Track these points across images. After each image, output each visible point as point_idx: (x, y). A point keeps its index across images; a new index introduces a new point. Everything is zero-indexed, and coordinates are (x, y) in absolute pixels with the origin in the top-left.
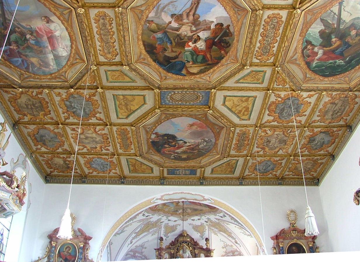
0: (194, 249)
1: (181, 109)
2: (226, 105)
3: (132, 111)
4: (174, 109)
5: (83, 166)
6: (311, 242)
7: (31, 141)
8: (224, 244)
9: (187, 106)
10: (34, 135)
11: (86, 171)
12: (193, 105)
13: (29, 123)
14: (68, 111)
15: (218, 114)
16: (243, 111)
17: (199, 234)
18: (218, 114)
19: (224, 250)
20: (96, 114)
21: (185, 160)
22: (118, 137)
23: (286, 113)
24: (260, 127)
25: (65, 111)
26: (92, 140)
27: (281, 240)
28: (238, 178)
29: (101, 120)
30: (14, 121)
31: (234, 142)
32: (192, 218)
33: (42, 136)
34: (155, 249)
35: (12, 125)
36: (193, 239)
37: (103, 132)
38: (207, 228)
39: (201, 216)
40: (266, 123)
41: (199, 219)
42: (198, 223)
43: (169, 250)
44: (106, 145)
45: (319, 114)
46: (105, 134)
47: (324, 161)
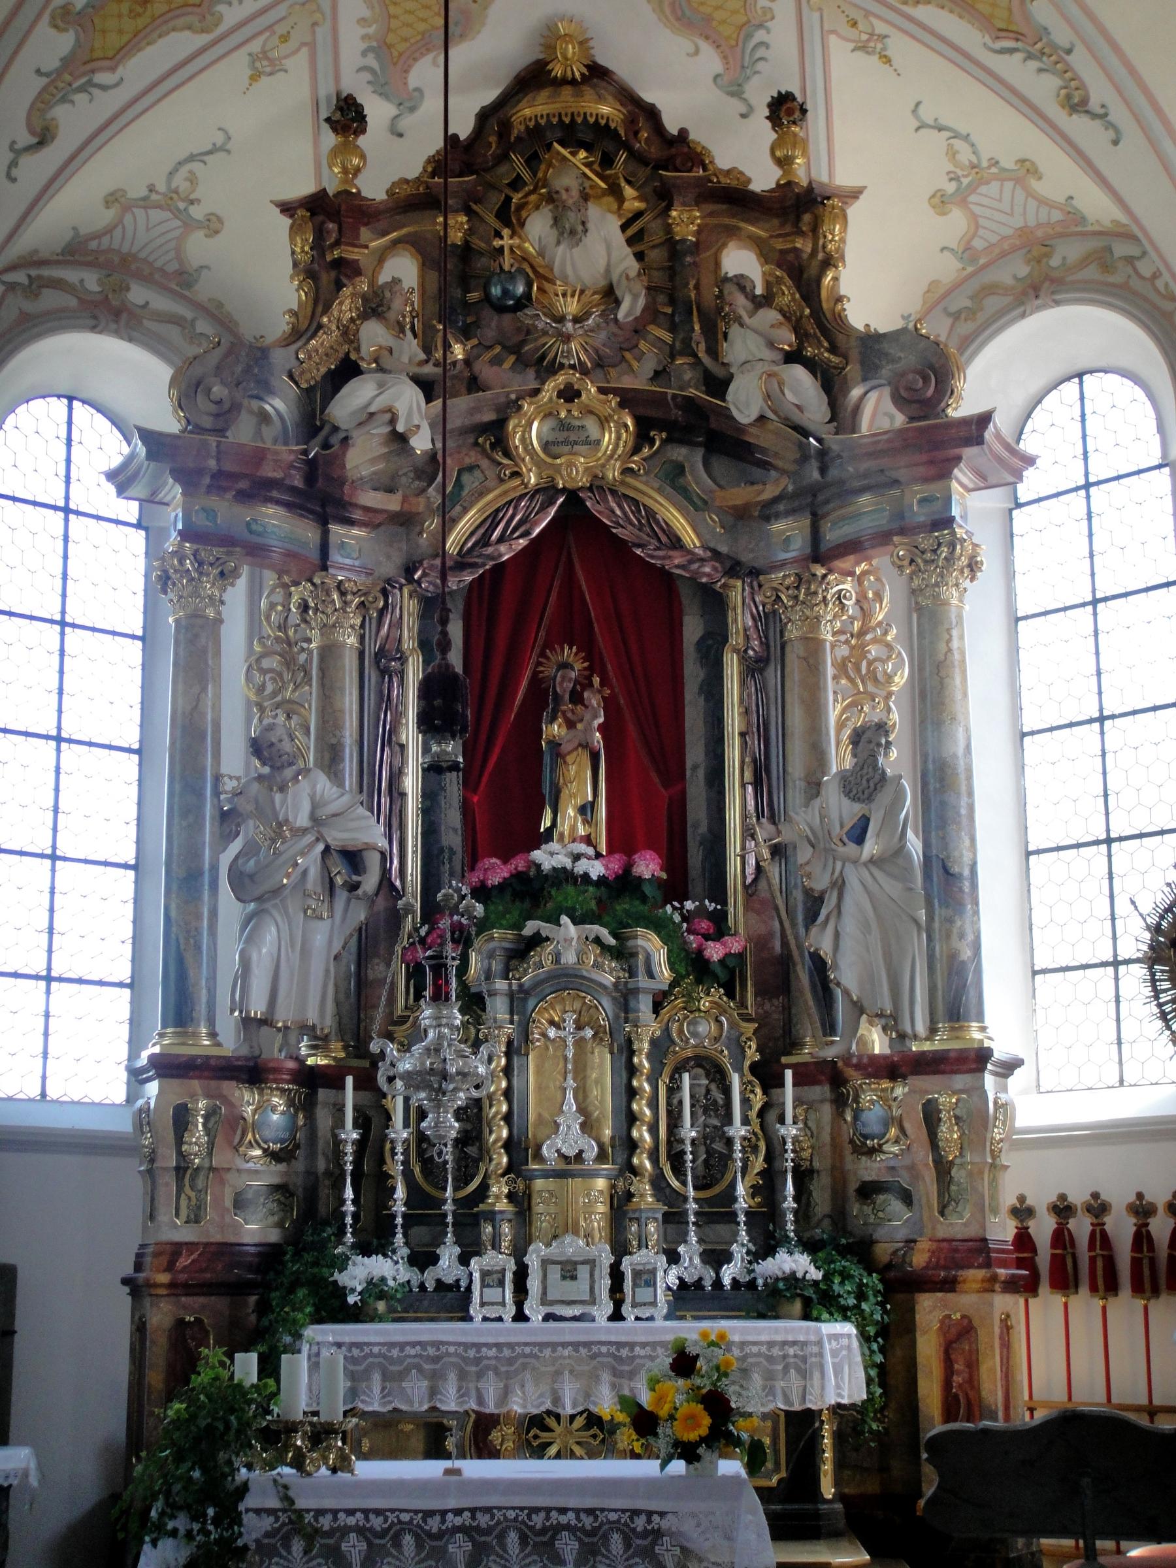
0: (663, 197)
8: (952, 154)
17: (710, 61)
19: (956, 223)
34: (287, 208)
36: (652, 114)
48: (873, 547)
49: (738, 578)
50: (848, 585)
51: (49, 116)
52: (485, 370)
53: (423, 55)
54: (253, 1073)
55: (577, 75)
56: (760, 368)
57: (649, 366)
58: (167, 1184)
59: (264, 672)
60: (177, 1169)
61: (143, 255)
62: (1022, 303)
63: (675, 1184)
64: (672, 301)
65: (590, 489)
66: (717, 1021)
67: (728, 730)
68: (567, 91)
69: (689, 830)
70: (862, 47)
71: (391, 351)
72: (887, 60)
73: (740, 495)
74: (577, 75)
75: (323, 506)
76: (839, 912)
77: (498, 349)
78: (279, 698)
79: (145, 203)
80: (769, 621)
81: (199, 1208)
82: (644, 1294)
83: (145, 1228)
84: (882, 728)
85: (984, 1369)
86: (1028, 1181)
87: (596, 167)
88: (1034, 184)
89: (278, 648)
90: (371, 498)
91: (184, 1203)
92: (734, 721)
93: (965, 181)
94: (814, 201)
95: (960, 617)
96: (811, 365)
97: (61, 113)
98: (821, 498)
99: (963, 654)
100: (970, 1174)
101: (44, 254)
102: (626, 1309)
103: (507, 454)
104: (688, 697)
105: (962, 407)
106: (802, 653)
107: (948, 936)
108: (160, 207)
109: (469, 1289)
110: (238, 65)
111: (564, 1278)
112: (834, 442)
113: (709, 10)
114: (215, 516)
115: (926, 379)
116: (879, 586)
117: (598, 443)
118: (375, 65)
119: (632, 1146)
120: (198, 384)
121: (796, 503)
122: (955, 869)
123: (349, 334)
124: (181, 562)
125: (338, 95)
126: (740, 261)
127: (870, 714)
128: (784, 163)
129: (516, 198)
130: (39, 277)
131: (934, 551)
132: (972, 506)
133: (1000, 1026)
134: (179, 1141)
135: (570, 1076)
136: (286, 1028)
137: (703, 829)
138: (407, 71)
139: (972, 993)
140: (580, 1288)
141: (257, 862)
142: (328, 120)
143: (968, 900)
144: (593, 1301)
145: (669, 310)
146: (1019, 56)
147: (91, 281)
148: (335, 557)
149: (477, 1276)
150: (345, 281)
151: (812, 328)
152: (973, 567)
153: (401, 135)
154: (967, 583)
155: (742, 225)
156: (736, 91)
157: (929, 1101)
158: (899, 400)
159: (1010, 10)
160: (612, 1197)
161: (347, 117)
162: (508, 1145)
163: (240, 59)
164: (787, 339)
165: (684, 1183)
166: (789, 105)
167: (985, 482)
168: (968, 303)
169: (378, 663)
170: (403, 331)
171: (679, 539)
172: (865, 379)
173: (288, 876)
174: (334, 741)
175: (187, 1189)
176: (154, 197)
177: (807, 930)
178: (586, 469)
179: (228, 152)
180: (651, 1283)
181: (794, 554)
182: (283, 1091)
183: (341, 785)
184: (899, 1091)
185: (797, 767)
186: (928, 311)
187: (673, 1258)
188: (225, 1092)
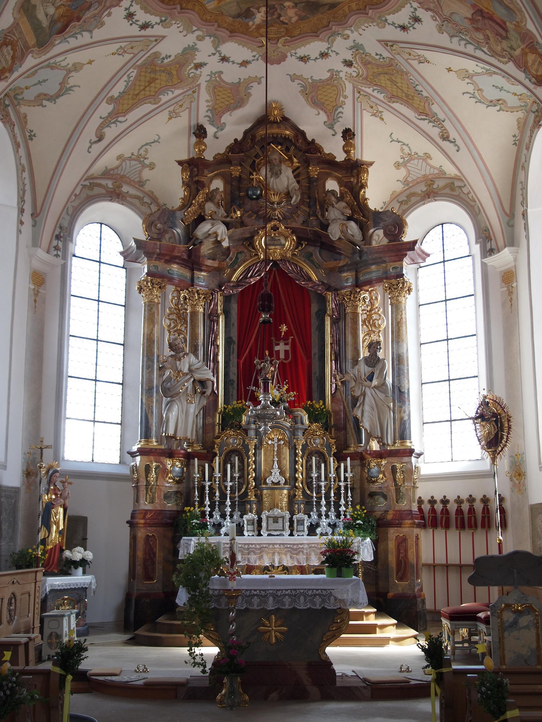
0: (307, 163)
8: (402, 150)
17: (323, 117)
19: (402, 172)
32: (301, 52)
34: (180, 163)
36: (303, 133)
38: (349, 87)
39: (330, 39)
41: (324, 55)
42: (318, 71)
48: (376, 283)
49: (330, 291)
50: (367, 295)
51: (103, 131)
52: (246, 220)
53: (226, 112)
54: (171, 455)
55: (279, 121)
56: (340, 222)
57: (301, 220)
58: (143, 491)
59: (170, 319)
60: (146, 485)
61: (127, 176)
62: (424, 200)
63: (309, 492)
64: (309, 198)
65: (281, 260)
66: (323, 438)
67: (326, 342)
68: (275, 125)
69: (313, 375)
70: (374, 115)
71: (216, 213)
72: (383, 119)
73: (332, 264)
74: (279, 121)
75: (193, 265)
76: (364, 404)
77: (250, 212)
78: (175, 329)
79: (130, 159)
80: (341, 307)
81: (153, 498)
82: (300, 528)
83: (134, 505)
84: (378, 343)
85: (409, 552)
86: (424, 491)
87: (284, 151)
88: (429, 161)
89: (175, 312)
90: (209, 263)
91: (148, 497)
92: (328, 339)
93: (406, 159)
94: (358, 166)
95: (405, 307)
96: (356, 221)
97: (106, 130)
98: (359, 266)
99: (406, 319)
100: (407, 489)
101: (95, 175)
102: (295, 532)
103: (254, 248)
104: (313, 331)
105: (407, 238)
106: (352, 317)
107: (400, 412)
108: (135, 160)
109: (243, 526)
110: (165, 115)
111: (274, 522)
112: (365, 248)
113: (324, 101)
114: (158, 268)
115: (395, 228)
116: (376, 295)
117: (284, 245)
118: (210, 115)
119: (296, 479)
120: (152, 223)
121: (351, 267)
122: (403, 390)
123: (201, 206)
124: (147, 284)
125: (198, 124)
126: (332, 185)
127: (374, 338)
128: (347, 152)
129: (257, 161)
130: (93, 183)
131: (397, 285)
132: (408, 269)
133: (415, 442)
134: (147, 476)
135: (275, 457)
136: (180, 439)
137: (317, 375)
138: (221, 117)
139: (408, 431)
140: (279, 525)
141: (171, 384)
142: (194, 133)
143: (407, 400)
144: (283, 530)
145: (308, 201)
146: (427, 121)
147: (110, 184)
148: (196, 281)
149: (245, 522)
150: (200, 188)
151: (357, 209)
152: (409, 290)
153: (217, 138)
154: (407, 296)
155: (333, 172)
156: (331, 127)
157: (393, 466)
158: (386, 234)
159: (425, 107)
160: (289, 496)
161: (200, 132)
162: (255, 479)
163: (166, 112)
164: (348, 212)
165: (312, 492)
166: (349, 133)
167: (414, 262)
168: (405, 199)
169: (210, 318)
170: (219, 206)
171: (311, 278)
172: (374, 227)
173: (182, 389)
174: (195, 344)
175: (149, 492)
176: (133, 157)
177: (353, 409)
178: (280, 253)
179: (159, 142)
180: (303, 524)
181: (350, 284)
182: (180, 460)
183: (198, 359)
184: (384, 462)
186: (391, 201)
187: (309, 516)
188: (162, 460)
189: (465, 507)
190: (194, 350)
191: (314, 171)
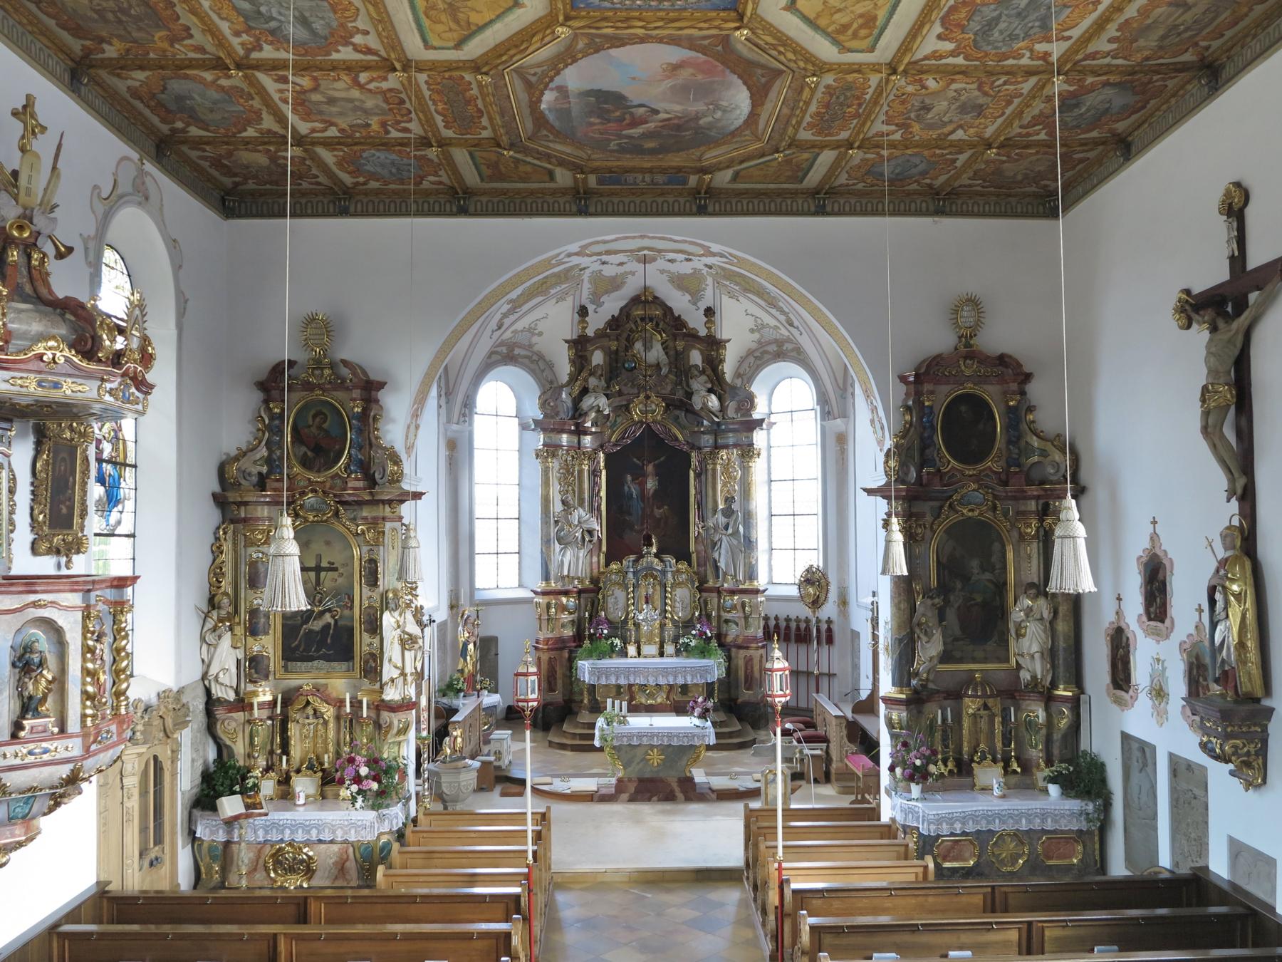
0: (675, 337)
1: (641, 24)
2: (797, 10)
3: (474, 28)
4: (619, 24)
5: (334, 168)
6: (1014, 393)
7: (147, 112)
9: (662, 14)
10: (153, 96)
11: (347, 179)
12: (685, 9)
13: (122, 62)
14: (250, 28)
15: (769, 39)
16: (855, 25)
17: (688, 297)
18: (769, 39)
19: (756, 336)
20: (352, 36)
21: (653, 152)
22: (436, 97)
23: (1001, 32)
24: (905, 72)
25: (238, 27)
26: (350, 105)
27: (927, 387)
28: (814, 193)
29: (369, 51)
30: (72, 60)
31: (813, 108)
33: (180, 99)
34: (566, 341)
35: (67, 77)
36: (670, 309)
37: (385, 85)
38: (710, 280)
40: (926, 58)
43: (605, 342)
44: (399, 118)
45: (1118, 34)
46: (391, 90)
47: (1091, 155)
54: (566, 593)
105: (756, 415)
119: (666, 611)
123: (586, 380)
161: (583, 312)
185: (710, 505)
189: (803, 626)
190: (581, 504)
191: (680, 345)
